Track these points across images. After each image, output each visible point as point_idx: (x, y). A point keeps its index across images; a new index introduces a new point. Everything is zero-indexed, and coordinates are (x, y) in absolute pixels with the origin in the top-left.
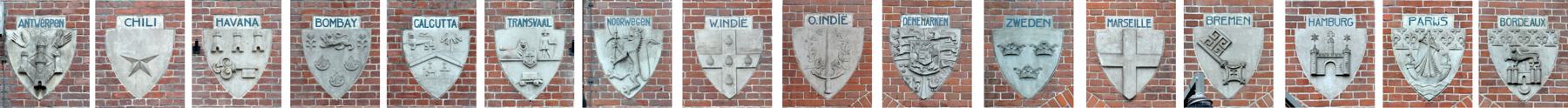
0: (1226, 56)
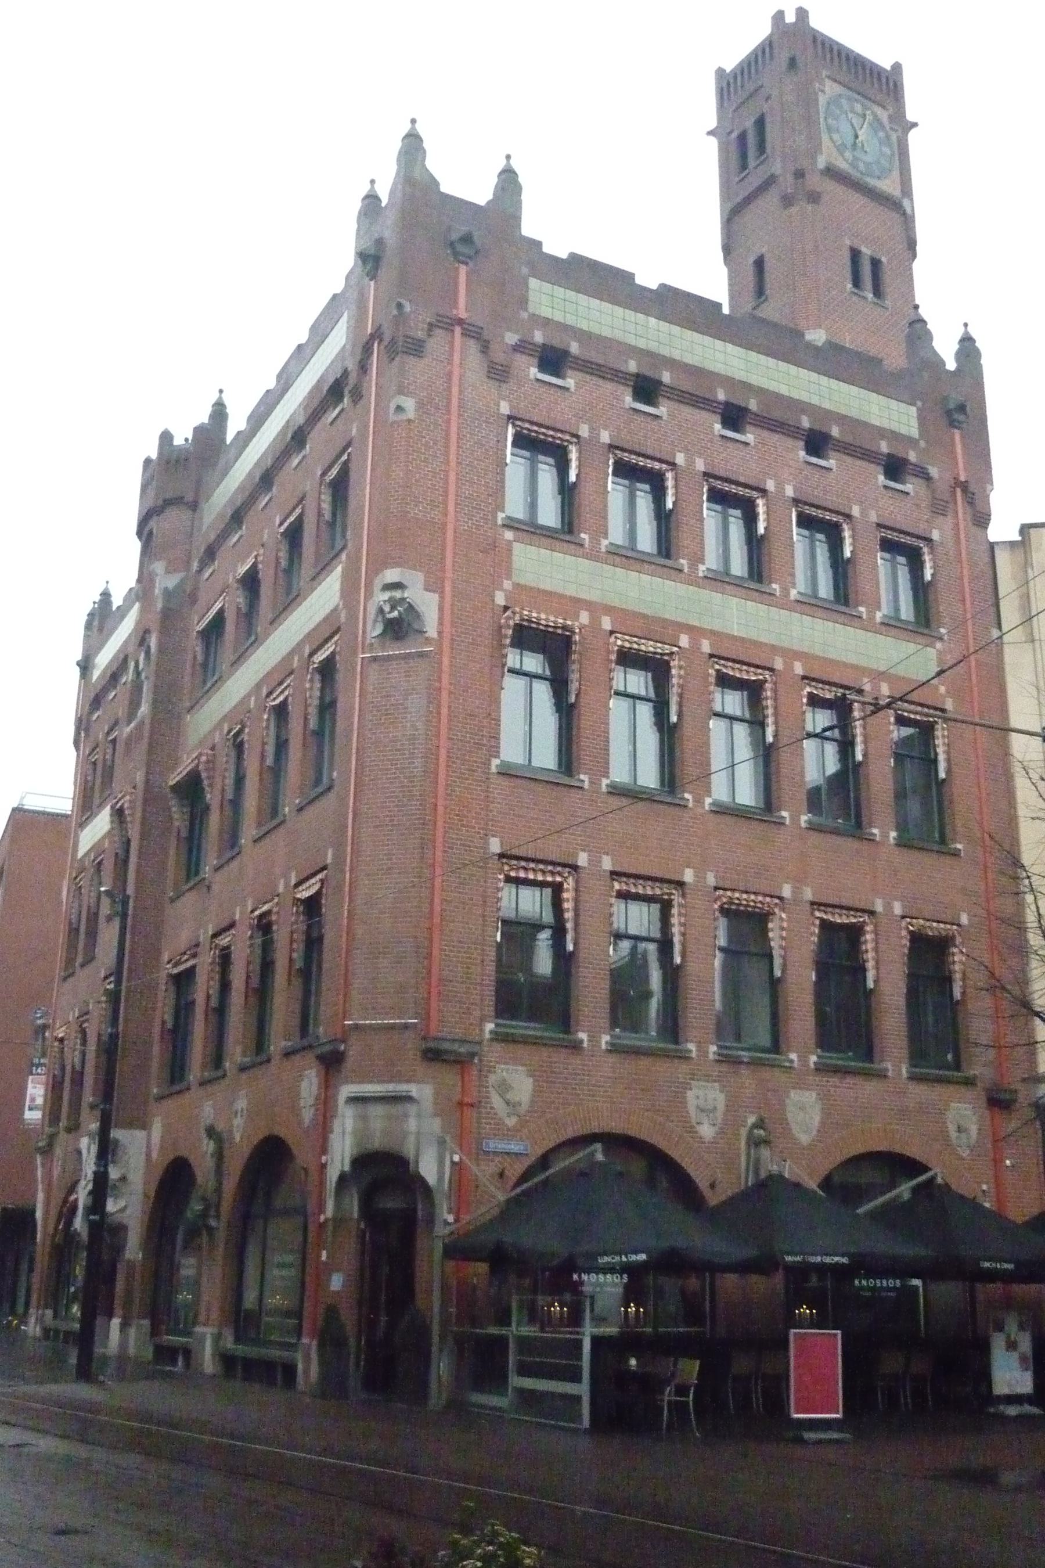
0: (508, 1096)
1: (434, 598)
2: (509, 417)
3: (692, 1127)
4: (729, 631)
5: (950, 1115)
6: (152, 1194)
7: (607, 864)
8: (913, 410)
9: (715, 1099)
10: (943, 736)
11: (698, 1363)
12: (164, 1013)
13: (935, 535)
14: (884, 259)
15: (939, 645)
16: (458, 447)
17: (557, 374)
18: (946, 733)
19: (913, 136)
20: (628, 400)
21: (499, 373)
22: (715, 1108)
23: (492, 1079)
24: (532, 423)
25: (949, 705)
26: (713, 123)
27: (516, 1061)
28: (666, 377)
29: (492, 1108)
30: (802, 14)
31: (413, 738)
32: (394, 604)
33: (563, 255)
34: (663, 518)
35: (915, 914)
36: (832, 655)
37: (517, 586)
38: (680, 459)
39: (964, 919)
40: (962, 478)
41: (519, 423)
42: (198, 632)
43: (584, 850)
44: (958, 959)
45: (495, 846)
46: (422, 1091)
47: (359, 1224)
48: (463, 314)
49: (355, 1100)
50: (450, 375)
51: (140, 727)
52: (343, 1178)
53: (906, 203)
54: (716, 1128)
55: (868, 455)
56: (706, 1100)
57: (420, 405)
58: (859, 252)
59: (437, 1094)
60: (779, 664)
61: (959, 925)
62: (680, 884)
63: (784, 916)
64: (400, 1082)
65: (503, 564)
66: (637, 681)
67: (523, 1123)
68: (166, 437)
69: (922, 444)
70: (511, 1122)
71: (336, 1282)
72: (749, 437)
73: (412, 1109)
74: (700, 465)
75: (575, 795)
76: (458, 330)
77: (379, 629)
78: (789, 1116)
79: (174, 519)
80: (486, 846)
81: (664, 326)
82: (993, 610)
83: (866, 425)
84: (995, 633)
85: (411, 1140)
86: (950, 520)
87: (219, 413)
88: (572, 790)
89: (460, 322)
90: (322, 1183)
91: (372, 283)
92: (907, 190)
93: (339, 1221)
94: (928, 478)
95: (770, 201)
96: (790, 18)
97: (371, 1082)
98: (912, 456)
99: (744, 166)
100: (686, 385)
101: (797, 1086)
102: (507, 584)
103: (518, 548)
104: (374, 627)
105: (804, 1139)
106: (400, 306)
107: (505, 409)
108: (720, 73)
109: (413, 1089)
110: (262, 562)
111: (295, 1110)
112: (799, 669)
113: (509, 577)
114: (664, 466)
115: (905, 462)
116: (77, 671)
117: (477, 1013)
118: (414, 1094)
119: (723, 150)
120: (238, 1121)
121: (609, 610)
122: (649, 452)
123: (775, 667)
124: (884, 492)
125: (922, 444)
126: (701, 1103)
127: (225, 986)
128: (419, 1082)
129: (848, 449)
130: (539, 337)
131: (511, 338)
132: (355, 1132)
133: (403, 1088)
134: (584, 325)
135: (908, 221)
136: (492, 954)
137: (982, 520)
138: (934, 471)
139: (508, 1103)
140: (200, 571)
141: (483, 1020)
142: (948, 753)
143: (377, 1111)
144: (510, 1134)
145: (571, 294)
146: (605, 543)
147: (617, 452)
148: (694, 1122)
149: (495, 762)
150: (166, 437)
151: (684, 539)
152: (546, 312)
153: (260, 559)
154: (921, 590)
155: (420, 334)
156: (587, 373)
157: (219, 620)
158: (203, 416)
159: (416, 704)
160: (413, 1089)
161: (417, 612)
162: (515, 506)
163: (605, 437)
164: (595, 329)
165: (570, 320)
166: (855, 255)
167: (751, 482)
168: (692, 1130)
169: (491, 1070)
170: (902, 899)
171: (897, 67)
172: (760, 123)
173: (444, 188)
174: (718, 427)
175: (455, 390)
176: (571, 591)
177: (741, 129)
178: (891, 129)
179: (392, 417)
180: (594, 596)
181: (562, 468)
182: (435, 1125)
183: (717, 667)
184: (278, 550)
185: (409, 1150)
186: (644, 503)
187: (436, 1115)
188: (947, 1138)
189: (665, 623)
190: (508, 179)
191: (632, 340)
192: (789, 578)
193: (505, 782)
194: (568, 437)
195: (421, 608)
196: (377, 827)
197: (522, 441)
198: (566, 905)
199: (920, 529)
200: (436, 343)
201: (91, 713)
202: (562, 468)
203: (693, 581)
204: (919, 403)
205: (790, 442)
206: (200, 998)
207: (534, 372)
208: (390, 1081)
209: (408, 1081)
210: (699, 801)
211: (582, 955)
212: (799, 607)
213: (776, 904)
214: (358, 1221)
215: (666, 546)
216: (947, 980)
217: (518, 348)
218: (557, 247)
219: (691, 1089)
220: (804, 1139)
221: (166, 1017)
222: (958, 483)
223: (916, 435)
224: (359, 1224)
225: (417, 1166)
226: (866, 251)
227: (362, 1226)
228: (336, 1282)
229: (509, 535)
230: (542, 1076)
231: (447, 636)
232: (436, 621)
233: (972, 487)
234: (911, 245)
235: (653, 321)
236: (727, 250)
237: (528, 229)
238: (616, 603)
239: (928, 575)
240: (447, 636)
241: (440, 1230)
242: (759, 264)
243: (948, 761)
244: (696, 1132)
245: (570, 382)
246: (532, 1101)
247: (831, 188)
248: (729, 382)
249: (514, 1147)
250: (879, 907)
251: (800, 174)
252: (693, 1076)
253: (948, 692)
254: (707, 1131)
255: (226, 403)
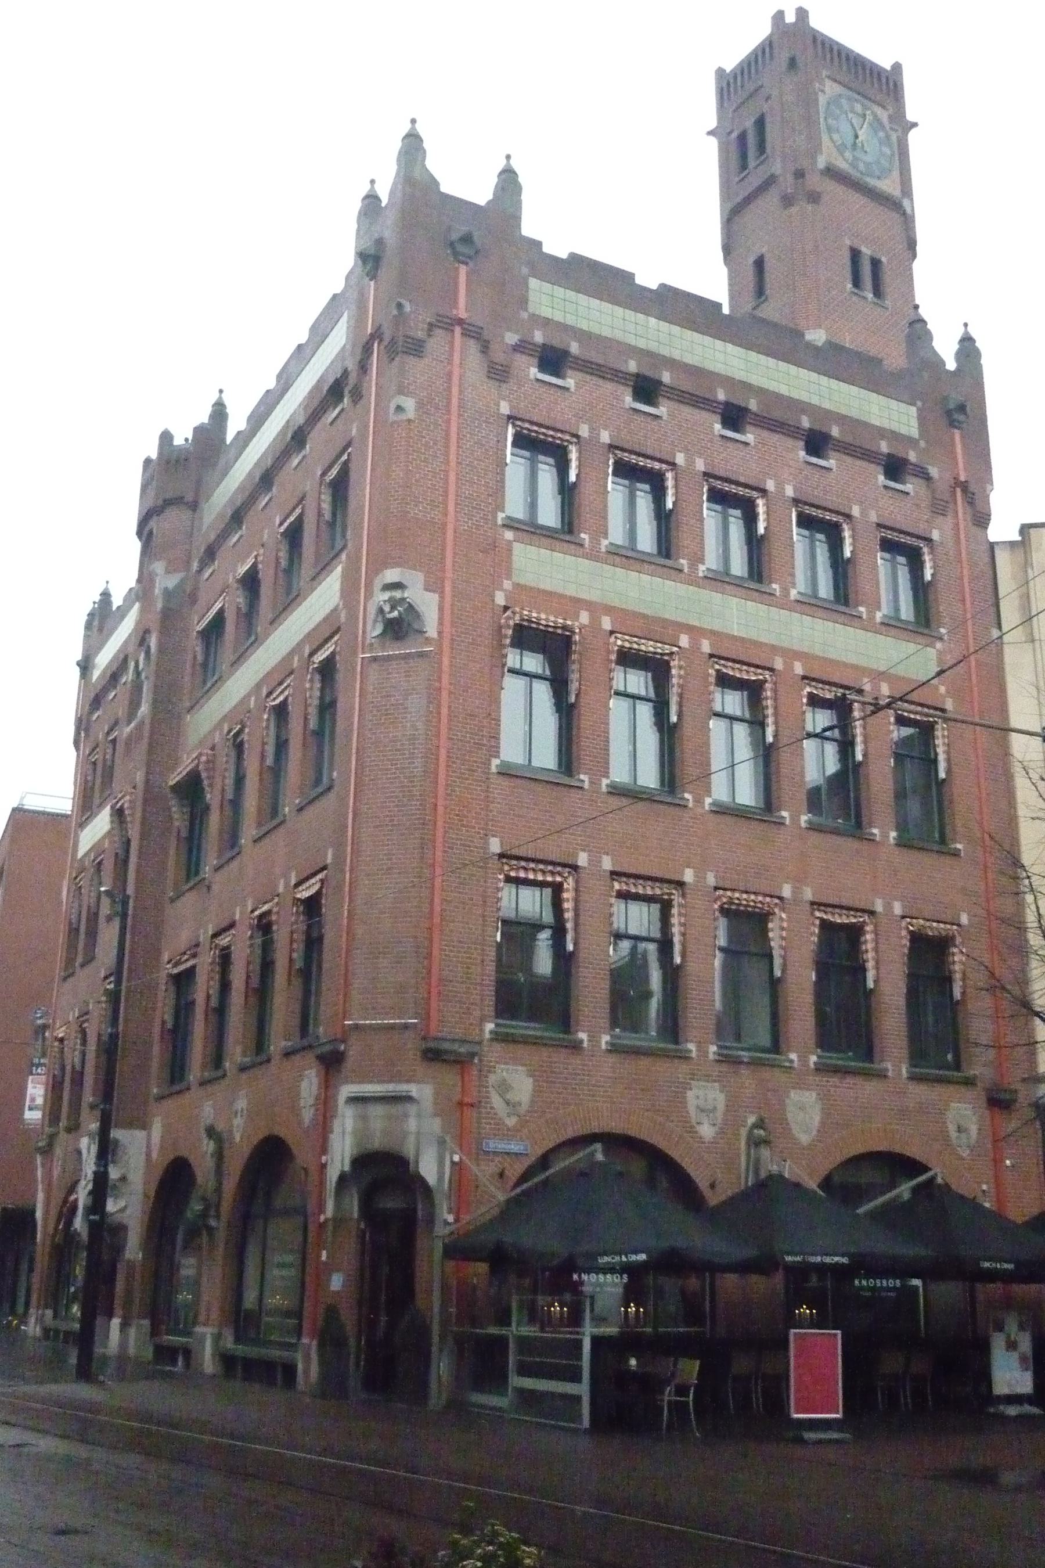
0: (508, 1096)
1: (434, 598)
2: (509, 417)
3: (692, 1127)
4: (729, 631)
5: (950, 1115)
6: (152, 1194)
7: (607, 864)
8: (913, 410)
9: (715, 1099)
10: (943, 736)
11: (698, 1363)
12: (164, 1013)
13: (935, 535)
14: (884, 259)
15: (939, 645)
16: (458, 447)
17: (557, 374)
18: (946, 733)
19: (913, 136)
20: (628, 400)
21: (499, 373)
22: (715, 1108)
23: (492, 1079)
24: (532, 423)
25: (949, 705)
26: (713, 123)
27: (516, 1061)
28: (666, 377)
29: (492, 1108)
30: (802, 14)
31: (413, 738)
32: (394, 604)
33: (563, 255)
34: (663, 518)
35: (915, 914)
36: (832, 655)
37: (517, 586)
38: (680, 459)
39: (964, 919)
40: (962, 478)
41: (519, 423)
42: (198, 632)
43: (584, 850)
44: (958, 959)
45: (495, 846)
46: (422, 1091)
47: (359, 1224)
48: (463, 314)
49: (355, 1100)
50: (450, 375)
51: (140, 727)
52: (343, 1178)
53: (906, 203)
54: (716, 1128)
55: (868, 455)
56: (706, 1100)
57: (420, 405)
58: (859, 252)
59: (437, 1094)
60: (779, 664)
61: (959, 925)
62: (680, 884)
63: (784, 916)
64: (400, 1082)
65: (503, 564)
66: (637, 681)
67: (523, 1123)
68: (166, 437)
69: (922, 444)
70: (511, 1122)
71: (336, 1282)
72: (749, 437)
73: (412, 1109)
74: (700, 465)
75: (575, 795)
76: (458, 330)
77: (379, 629)
78: (789, 1116)
79: (174, 519)
80: (486, 846)
81: (664, 326)
82: (993, 610)
83: (866, 425)
84: (995, 633)
85: (411, 1140)
86: (950, 520)
87: (219, 413)
88: (572, 790)
89: (460, 322)
90: (322, 1183)
91: (372, 283)
92: (907, 190)
93: (339, 1221)
94: (928, 478)
95: (770, 201)
96: (790, 18)
97: (371, 1082)
98: (912, 456)
99: (744, 166)
100: (686, 385)
101: (797, 1086)
102: (507, 584)
103: (518, 548)
104: (374, 627)
105: (804, 1139)
106: (400, 306)
107: (505, 409)
108: (720, 73)
109: (413, 1089)
110: (262, 562)
111: (295, 1110)
112: (799, 669)
113: (509, 577)
114: (664, 466)
115: (905, 462)
116: (77, 671)
117: (477, 1013)
118: (414, 1094)
119: (723, 150)
120: (238, 1121)
121: (609, 610)
122: (649, 452)
123: (775, 667)
124: (884, 492)
125: (922, 444)
126: (701, 1103)
127: (225, 986)
128: (419, 1082)
129: (848, 449)
130: (539, 337)
131: (511, 338)
132: (355, 1132)
133: (403, 1088)
134: (584, 325)
135: (908, 221)
136: (492, 954)
137: (982, 520)
138: (934, 471)
139: (508, 1103)
140: (200, 571)
141: (483, 1020)
142: (948, 753)
143: (377, 1111)
144: (510, 1134)
145: (571, 294)
146: (605, 543)
147: (617, 452)
148: (694, 1122)
149: (495, 762)
150: (166, 437)
151: (684, 539)
152: (546, 312)
153: (260, 559)
154: (921, 590)
155: (420, 334)
156: (587, 373)
157: (219, 620)
158: (203, 416)
159: (416, 704)
160: (413, 1089)
161: (417, 612)
162: (515, 506)
163: (605, 437)
164: (595, 329)
165: (570, 320)
166: (855, 255)
167: (751, 482)
168: (692, 1130)
169: (491, 1070)
170: (902, 899)
171: (897, 67)
172: (760, 123)
173: (444, 188)
174: (718, 427)
175: (455, 390)
176: (571, 591)
177: (741, 129)
178: (891, 129)
179: (392, 417)
180: (594, 596)
181: (562, 468)
182: (435, 1125)
183: (717, 667)
184: (278, 550)
185: (409, 1150)
186: (644, 503)
187: (436, 1115)
188: (947, 1138)
189: (665, 623)
190: (508, 179)
191: (632, 340)
192: (789, 578)
193: (505, 782)
194: (568, 437)
195: (421, 608)
196: (377, 827)
197: (522, 441)
198: (566, 905)
199: (920, 529)
200: (436, 343)
201: (91, 713)
202: (562, 468)
203: (693, 581)
204: (919, 403)
205: (790, 442)
206: (200, 998)
207: (534, 372)
208: (390, 1081)
209: (408, 1081)
210: (699, 801)
211: (582, 955)
212: (799, 607)
213: (776, 904)
214: (358, 1221)
215: (666, 546)
216: (947, 980)
217: (518, 348)
218: (557, 247)
219: (691, 1089)
220: (804, 1139)
221: (166, 1017)
222: (958, 483)
223: (916, 435)
224: (359, 1224)
225: (417, 1166)
226: (866, 251)
227: (362, 1226)
228: (336, 1282)
229: (509, 535)
230: (542, 1076)
231: (447, 636)
232: (436, 621)
233: (972, 487)
234: (911, 245)
235: (653, 321)
236: (727, 250)
237: (528, 229)
238: (616, 603)
239: (928, 575)
240: (447, 636)
241: (440, 1230)
242: (759, 264)
243: (948, 761)
244: (696, 1132)
245: (570, 382)
246: (532, 1101)
247: (831, 188)
248: (729, 382)
249: (514, 1147)
250: (879, 907)
251: (800, 174)
252: (693, 1076)
253: (948, 692)
254: (707, 1131)
255: (226, 403)
